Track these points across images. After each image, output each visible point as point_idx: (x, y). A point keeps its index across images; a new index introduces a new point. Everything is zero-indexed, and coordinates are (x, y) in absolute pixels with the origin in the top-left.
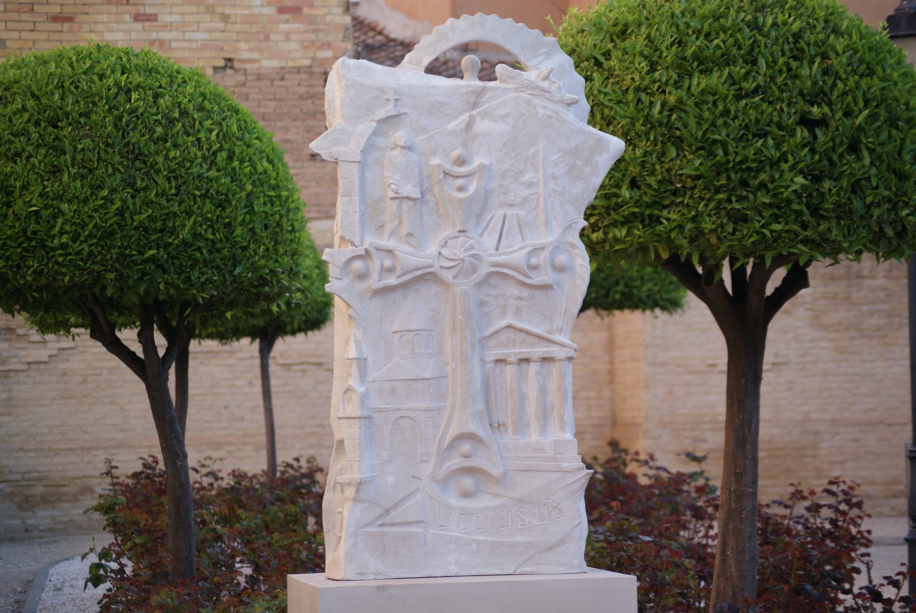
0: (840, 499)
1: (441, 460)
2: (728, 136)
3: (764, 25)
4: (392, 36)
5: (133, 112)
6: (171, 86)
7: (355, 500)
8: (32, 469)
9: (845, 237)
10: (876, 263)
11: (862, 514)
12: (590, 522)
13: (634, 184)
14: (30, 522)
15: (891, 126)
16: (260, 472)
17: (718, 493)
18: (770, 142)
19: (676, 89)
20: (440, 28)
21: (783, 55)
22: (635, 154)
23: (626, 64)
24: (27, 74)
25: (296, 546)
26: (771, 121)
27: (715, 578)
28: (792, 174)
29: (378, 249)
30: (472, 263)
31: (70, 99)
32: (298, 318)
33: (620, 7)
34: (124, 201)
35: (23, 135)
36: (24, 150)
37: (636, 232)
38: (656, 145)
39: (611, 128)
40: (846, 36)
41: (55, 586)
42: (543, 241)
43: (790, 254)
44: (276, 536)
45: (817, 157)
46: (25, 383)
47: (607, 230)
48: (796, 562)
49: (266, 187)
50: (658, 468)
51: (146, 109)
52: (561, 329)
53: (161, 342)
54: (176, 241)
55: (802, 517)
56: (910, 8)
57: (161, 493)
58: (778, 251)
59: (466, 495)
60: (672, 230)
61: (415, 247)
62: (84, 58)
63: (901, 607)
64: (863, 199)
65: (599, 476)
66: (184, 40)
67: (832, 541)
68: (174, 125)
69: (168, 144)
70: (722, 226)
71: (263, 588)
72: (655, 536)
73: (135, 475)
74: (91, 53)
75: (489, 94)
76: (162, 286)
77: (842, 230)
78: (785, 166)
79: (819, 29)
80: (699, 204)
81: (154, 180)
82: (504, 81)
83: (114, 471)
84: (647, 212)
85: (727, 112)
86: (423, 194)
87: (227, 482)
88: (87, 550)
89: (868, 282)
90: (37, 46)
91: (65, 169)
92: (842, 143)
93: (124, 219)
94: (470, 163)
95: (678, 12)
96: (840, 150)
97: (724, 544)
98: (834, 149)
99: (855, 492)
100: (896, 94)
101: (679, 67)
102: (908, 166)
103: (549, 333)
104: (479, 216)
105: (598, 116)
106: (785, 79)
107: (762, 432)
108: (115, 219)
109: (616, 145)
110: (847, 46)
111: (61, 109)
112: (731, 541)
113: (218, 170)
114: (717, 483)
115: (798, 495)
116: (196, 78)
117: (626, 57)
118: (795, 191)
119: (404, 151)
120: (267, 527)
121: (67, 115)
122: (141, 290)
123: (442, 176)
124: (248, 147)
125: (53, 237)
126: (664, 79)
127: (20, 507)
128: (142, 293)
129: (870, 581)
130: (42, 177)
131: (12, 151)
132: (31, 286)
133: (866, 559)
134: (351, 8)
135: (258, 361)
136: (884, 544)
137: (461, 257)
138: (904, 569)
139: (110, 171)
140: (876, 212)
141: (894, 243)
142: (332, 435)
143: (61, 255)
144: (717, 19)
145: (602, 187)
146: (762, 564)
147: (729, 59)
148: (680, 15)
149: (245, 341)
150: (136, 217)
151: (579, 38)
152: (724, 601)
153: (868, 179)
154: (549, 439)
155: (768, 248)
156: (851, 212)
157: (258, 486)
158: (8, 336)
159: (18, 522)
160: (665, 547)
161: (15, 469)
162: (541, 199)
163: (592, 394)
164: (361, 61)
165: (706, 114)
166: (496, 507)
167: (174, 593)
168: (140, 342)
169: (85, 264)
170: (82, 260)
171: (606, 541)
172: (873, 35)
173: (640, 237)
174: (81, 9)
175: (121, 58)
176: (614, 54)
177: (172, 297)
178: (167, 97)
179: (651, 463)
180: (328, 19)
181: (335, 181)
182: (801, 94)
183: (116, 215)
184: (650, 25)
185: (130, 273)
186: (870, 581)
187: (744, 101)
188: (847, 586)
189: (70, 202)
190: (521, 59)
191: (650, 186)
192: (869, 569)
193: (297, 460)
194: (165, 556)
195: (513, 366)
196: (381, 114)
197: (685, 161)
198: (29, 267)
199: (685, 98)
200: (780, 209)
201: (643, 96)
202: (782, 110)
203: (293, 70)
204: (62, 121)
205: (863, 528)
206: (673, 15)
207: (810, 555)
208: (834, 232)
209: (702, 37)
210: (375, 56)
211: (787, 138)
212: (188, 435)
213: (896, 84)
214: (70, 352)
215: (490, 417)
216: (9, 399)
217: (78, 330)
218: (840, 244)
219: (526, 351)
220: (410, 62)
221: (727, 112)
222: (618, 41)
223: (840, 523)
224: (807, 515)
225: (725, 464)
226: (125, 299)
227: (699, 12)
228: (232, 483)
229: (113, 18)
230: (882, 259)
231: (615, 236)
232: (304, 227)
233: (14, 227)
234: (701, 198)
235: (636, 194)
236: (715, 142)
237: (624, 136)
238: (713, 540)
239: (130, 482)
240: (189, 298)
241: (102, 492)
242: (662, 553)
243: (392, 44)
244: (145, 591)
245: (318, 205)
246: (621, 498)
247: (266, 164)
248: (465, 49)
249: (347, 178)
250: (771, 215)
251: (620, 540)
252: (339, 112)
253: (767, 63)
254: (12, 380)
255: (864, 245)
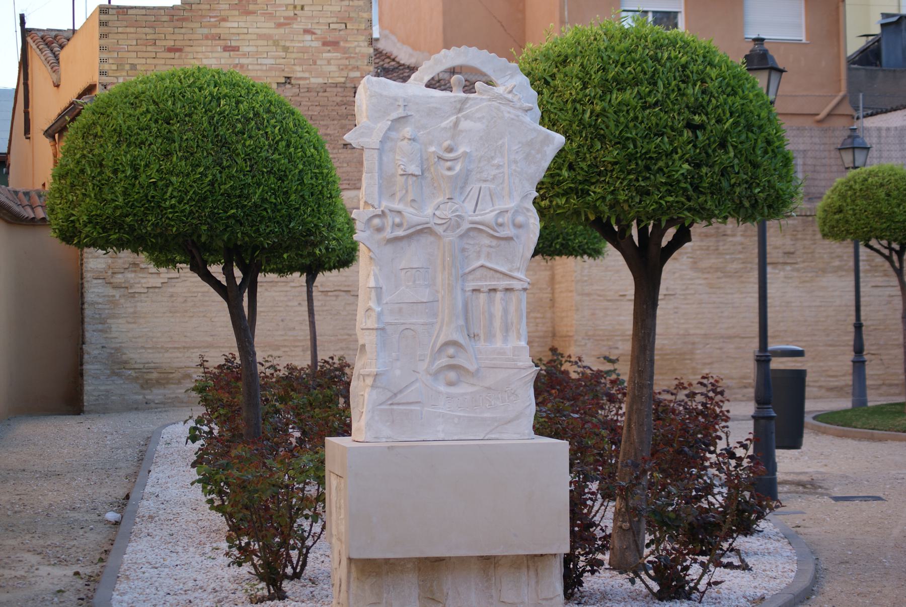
0: (709, 389)
1: (433, 359)
2: (637, 135)
3: (662, 58)
4: (402, 62)
5: (221, 114)
6: (248, 96)
7: (372, 386)
8: (150, 361)
9: (716, 207)
10: (737, 225)
11: (723, 399)
12: (537, 404)
13: (571, 167)
14: (148, 397)
15: (748, 130)
16: (306, 367)
17: (626, 384)
18: (666, 139)
19: (601, 101)
20: (436, 56)
21: (675, 79)
22: (572, 146)
23: (566, 83)
24: (150, 87)
25: (331, 418)
26: (667, 125)
27: (622, 443)
28: (681, 162)
29: (391, 211)
30: (457, 221)
31: (179, 105)
32: (334, 259)
33: (562, 44)
34: (214, 175)
35: (146, 129)
36: (147, 140)
37: (572, 201)
38: (587, 140)
39: (555, 128)
40: (717, 68)
41: (166, 441)
42: (507, 206)
43: (679, 218)
44: (317, 410)
45: (698, 151)
46: (146, 302)
47: (552, 199)
48: (678, 432)
49: (313, 166)
50: (584, 367)
51: (230, 111)
52: (519, 268)
53: (238, 274)
54: (250, 204)
55: (683, 401)
56: (760, 50)
57: (238, 379)
58: (671, 216)
59: (451, 384)
60: (597, 200)
61: (416, 209)
62: (189, 76)
63: (748, 463)
64: (729, 180)
65: (543, 372)
66: (258, 64)
67: (703, 418)
68: (249, 123)
69: (245, 136)
70: (632, 197)
71: (308, 446)
72: (581, 414)
73: (220, 367)
74: (194, 73)
75: (470, 102)
76: (239, 235)
77: (715, 202)
78: (676, 157)
79: (699, 62)
80: (616, 182)
81: (235, 161)
82: (480, 93)
83: (205, 363)
84: (580, 187)
85: (636, 118)
86: (423, 173)
87: (283, 372)
88: (188, 418)
89: (730, 239)
90: (158, 68)
91: (175, 153)
92: (715, 142)
93: (214, 188)
94: (456, 151)
95: (602, 48)
96: (714, 146)
97: (629, 420)
98: (709, 145)
99: (719, 385)
100: (752, 108)
101: (603, 86)
102: (760, 158)
103: (511, 271)
104: (462, 188)
105: (547, 120)
106: (676, 96)
107: (657, 342)
108: (208, 188)
109: (559, 139)
110: (718, 75)
111: (172, 111)
112: (635, 417)
113: (280, 154)
114: (625, 378)
115: (680, 386)
116: (265, 90)
117: (566, 78)
118: (683, 174)
119: (410, 142)
120: (311, 404)
121: (177, 115)
122: (225, 237)
123: (436, 160)
124: (301, 138)
125: (165, 200)
126: (593, 94)
127: (142, 387)
128: (226, 240)
129: (728, 445)
130: (159, 159)
131: (139, 141)
132: (150, 234)
133: (726, 429)
134: (373, 42)
135: (305, 289)
136: (737, 420)
137: (449, 216)
138: (751, 437)
139: (205, 154)
140: (738, 190)
141: (750, 211)
142: (357, 341)
143: (171, 213)
144: (630, 53)
145: (549, 169)
146: (655, 434)
147: (637, 81)
148: (604, 50)
149: (297, 274)
150: (222, 187)
151: (534, 65)
152: (628, 459)
153: (733, 167)
154: (510, 346)
155: (663, 214)
156: (721, 189)
157: (304, 376)
158: (133, 269)
159: (141, 397)
160: (588, 422)
161: (138, 361)
162: (506, 177)
163: (539, 315)
164: (381, 78)
165: (622, 119)
166: (471, 393)
167: (247, 449)
168: (224, 274)
169: (187, 219)
170: (185, 216)
171: (547, 417)
172: (736, 67)
173: (574, 205)
174: (188, 43)
175: (214, 76)
176: (558, 76)
177: (246, 243)
178: (245, 103)
179: (580, 364)
180: (357, 50)
181: (361, 163)
182: (687, 106)
183: (209, 185)
184: (583, 57)
185: (217, 225)
186: (728, 445)
187: (648, 111)
188: (712, 448)
189: (177, 175)
190: (493, 78)
191: (582, 169)
192: (727, 437)
193: (332, 358)
194: (240, 422)
195: (485, 294)
196: (394, 115)
197: (606, 152)
198: (149, 221)
199: (607, 108)
200: (672, 186)
201: (578, 106)
202: (674, 117)
203: (332, 85)
204: (173, 120)
205: (724, 409)
206: (599, 50)
207: (688, 427)
208: (709, 203)
209: (619, 66)
210: (390, 76)
211: (677, 137)
212: (256, 339)
213: (751, 101)
214: (176, 280)
215: (468, 330)
216: (135, 313)
217: (181, 265)
218: (713, 212)
219: (493, 283)
220: (415, 80)
221: (636, 118)
222: (561, 67)
223: (708, 406)
224: (686, 399)
225: (631, 364)
226: (214, 244)
227: (617, 48)
228: (287, 374)
229: (209, 49)
230: (741, 223)
231: (557, 203)
232: (339, 195)
233: (139, 193)
234: (618, 178)
235: (572, 174)
236: (628, 138)
237: (565, 133)
238: (622, 417)
239: (216, 371)
240: (258, 244)
241: (198, 378)
242: (586, 426)
243: (401, 68)
244: (226, 446)
245: (348, 180)
246: (558, 387)
247: (313, 150)
248: (453, 71)
249: (370, 160)
250: (666, 191)
251: (557, 417)
252: (365, 114)
253: (664, 85)
254: (136, 299)
255: (729, 213)
